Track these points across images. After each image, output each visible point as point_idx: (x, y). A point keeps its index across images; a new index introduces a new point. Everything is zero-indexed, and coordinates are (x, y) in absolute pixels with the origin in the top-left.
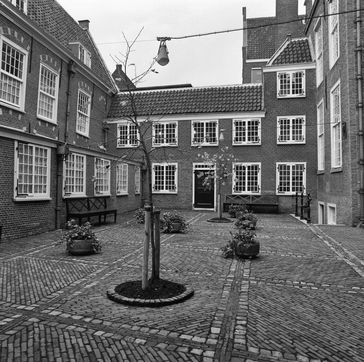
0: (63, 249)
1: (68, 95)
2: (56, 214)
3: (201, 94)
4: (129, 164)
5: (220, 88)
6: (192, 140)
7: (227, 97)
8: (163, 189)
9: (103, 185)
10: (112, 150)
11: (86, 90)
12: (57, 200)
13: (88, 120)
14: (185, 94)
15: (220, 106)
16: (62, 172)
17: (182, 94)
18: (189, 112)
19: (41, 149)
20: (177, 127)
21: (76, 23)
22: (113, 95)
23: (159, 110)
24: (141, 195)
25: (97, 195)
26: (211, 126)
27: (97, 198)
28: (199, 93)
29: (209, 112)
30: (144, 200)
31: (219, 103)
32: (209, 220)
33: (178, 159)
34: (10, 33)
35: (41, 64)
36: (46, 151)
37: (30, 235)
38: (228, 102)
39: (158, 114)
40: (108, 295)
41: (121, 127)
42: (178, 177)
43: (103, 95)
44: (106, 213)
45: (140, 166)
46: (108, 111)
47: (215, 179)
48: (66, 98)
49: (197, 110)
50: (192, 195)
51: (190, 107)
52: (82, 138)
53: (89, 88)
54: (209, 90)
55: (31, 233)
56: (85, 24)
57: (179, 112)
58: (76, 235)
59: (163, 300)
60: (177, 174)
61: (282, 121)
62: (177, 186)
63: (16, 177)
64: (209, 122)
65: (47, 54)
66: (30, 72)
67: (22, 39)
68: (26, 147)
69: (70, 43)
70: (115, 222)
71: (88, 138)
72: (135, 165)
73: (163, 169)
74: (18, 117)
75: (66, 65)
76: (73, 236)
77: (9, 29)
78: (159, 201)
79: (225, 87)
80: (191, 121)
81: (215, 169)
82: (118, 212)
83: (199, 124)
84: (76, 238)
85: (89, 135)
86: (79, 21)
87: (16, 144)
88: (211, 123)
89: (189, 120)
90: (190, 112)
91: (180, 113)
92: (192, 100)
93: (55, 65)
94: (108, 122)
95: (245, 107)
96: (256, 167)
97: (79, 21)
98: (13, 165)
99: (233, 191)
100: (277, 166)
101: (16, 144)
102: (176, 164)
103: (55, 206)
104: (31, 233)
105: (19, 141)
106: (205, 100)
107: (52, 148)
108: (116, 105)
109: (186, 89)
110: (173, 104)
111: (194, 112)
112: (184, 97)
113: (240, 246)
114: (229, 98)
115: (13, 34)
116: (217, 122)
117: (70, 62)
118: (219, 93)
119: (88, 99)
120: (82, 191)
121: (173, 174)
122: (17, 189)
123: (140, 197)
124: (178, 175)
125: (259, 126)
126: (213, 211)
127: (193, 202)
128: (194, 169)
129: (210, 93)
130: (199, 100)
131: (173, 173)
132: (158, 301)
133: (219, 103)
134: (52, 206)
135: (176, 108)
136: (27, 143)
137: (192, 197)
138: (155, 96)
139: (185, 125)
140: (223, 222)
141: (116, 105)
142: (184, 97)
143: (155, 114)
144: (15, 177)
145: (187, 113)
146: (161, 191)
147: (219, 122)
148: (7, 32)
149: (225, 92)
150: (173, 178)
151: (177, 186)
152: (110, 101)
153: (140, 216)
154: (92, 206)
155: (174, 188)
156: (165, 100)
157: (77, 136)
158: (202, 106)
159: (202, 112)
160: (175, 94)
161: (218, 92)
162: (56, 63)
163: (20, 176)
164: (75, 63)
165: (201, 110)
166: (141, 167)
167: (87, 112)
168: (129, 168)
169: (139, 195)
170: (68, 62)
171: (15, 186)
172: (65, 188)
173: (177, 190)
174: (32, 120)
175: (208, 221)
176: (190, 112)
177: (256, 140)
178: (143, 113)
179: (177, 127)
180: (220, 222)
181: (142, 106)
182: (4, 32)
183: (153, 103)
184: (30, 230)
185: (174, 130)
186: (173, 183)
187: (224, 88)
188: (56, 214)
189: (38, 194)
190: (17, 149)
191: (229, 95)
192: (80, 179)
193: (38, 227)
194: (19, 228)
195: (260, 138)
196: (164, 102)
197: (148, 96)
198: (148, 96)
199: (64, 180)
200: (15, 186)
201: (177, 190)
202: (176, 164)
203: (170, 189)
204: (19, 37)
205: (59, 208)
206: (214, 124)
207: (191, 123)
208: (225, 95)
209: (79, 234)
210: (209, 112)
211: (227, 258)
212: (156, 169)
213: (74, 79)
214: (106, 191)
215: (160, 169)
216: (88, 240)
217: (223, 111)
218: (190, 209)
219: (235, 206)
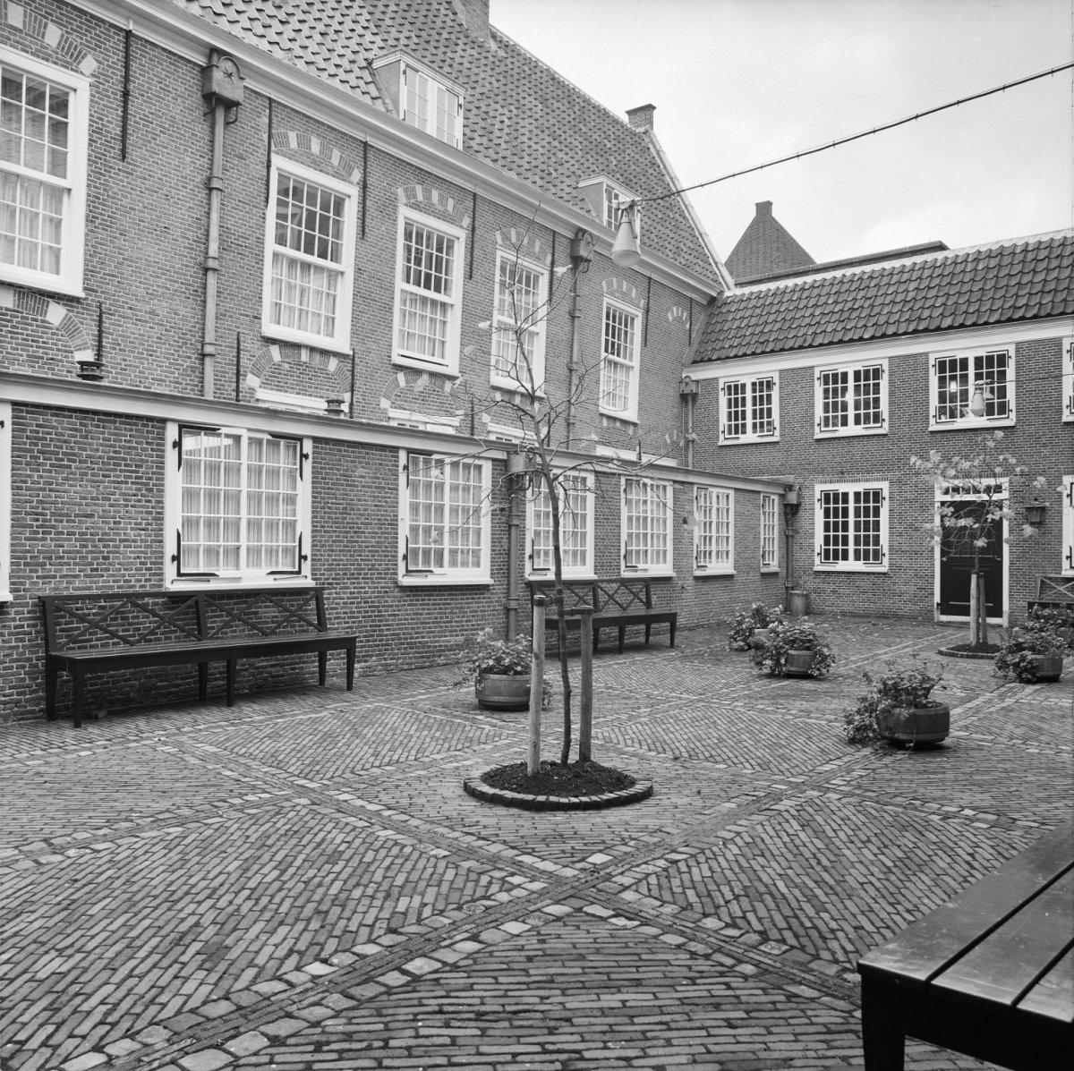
0: (468, 692)
1: (573, 317)
2: (507, 617)
3: (963, 271)
4: (736, 490)
5: (1027, 244)
6: (932, 412)
7: (1048, 270)
8: (845, 557)
9: (649, 548)
10: (705, 451)
11: (625, 297)
12: (508, 584)
13: (634, 378)
14: (915, 276)
15: (1022, 302)
16: (522, 516)
17: (906, 276)
18: (921, 328)
19: (467, 466)
20: (885, 376)
21: (616, 122)
22: (712, 300)
23: (835, 330)
24: (783, 574)
25: (626, 574)
26: (992, 366)
27: (625, 583)
28: (960, 268)
29: (986, 323)
30: (793, 588)
31: (1021, 293)
32: (943, 649)
33: (888, 470)
34: (420, 197)
35: (499, 254)
36: (479, 468)
37: (439, 665)
38: (1052, 286)
39: (831, 343)
40: (465, 784)
41: (729, 387)
42: (891, 523)
43: (678, 304)
44: (648, 620)
45: (780, 495)
46: (695, 346)
47: (1006, 524)
48: (567, 329)
49: (947, 322)
50: (933, 577)
51: (926, 313)
52: (618, 424)
53: (634, 291)
54: (990, 255)
55: (441, 661)
56: (641, 115)
57: (890, 331)
58: (491, 662)
59: (553, 799)
60: (887, 513)
61: (826, 377)
62: (886, 550)
63: (404, 531)
64: (984, 354)
65: (514, 226)
66: (471, 277)
67: (451, 203)
68: (427, 462)
69: (580, 185)
70: (672, 645)
71: (635, 425)
72: (758, 492)
73: (845, 500)
74: (443, 387)
75: (566, 242)
76: (484, 666)
77: (419, 189)
78: (834, 592)
79: (1045, 239)
80: (926, 354)
81: (1005, 495)
82: (681, 621)
83: (953, 362)
84: (490, 670)
85: (639, 415)
86: (629, 113)
87: (403, 455)
88: (990, 359)
89: (920, 354)
90: (926, 330)
91: (895, 334)
92: (933, 293)
93: (537, 249)
94: (695, 376)
95: (1041, 304)
96: (877, 495)
97: (629, 113)
98: (395, 505)
99: (817, 560)
100: (818, 496)
101: (403, 455)
102: (884, 486)
103: (504, 600)
104: (441, 661)
105: (410, 451)
106: (975, 289)
107: (494, 460)
108: (719, 327)
109: (929, 257)
110: (877, 310)
111: (938, 329)
112: (912, 286)
113: (884, 711)
114: (1055, 274)
115: (428, 197)
116: (1012, 353)
117: (576, 234)
118: (1023, 261)
119: (633, 319)
120: (665, 562)
121: (877, 513)
122: (405, 557)
123: (780, 582)
124: (891, 517)
125: (775, 394)
126: (1001, 626)
127: (937, 599)
128: (939, 497)
129: (993, 263)
130: (957, 288)
131: (877, 512)
132: (541, 798)
133: (1021, 293)
134: (497, 596)
135: (882, 320)
136: (430, 453)
137: (932, 583)
138: (826, 290)
139: (908, 369)
140: (982, 657)
141: (719, 327)
142: (912, 286)
143: (821, 345)
144: (400, 531)
145: (915, 331)
146: (842, 566)
147: (1017, 350)
148: (415, 196)
149: (1042, 255)
150: (877, 526)
151: (886, 550)
152: (700, 319)
153: (737, 632)
154: (606, 603)
155: (877, 555)
156: (855, 299)
157: (601, 422)
158: (964, 308)
159: (962, 326)
160: (885, 280)
161: (1020, 257)
162: (538, 244)
163: (414, 529)
164: (590, 234)
165: (960, 320)
166: (782, 496)
167: (631, 354)
168: (736, 501)
169: (775, 574)
170: (571, 236)
171: (402, 551)
172: (531, 557)
173: (886, 561)
174: (479, 392)
175: (941, 653)
176: (926, 330)
177: (876, 420)
178: (790, 344)
179: (885, 376)
180: (973, 657)
181: (787, 324)
182: (408, 197)
183: (817, 313)
184: (441, 651)
185: (877, 386)
186: (877, 540)
187: (1040, 243)
188: (507, 617)
189: (460, 570)
190: (406, 468)
191: (1055, 263)
192: (658, 536)
193: (459, 647)
194: (411, 645)
195: (1012, 405)
196: (849, 305)
197: (806, 294)
198: (806, 294)
199: (529, 536)
200: (402, 551)
201: (886, 561)
202: (884, 486)
203: (866, 558)
204: (442, 200)
205: (513, 604)
206: (1002, 360)
207: (927, 363)
208: (1043, 265)
209: (498, 660)
210: (986, 323)
211: (852, 741)
212: (827, 501)
213: (589, 274)
214: (658, 562)
215: (836, 501)
216: (518, 677)
217: (1029, 315)
218: (928, 619)
219: (1047, 612)
